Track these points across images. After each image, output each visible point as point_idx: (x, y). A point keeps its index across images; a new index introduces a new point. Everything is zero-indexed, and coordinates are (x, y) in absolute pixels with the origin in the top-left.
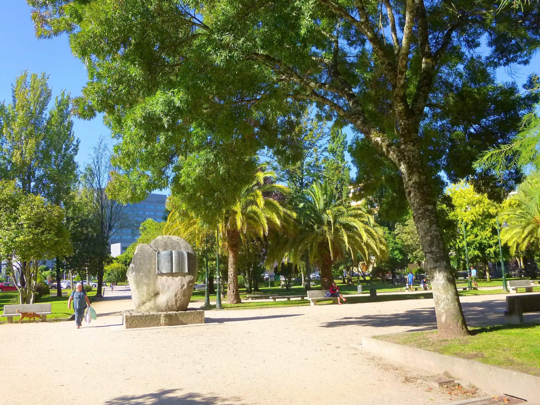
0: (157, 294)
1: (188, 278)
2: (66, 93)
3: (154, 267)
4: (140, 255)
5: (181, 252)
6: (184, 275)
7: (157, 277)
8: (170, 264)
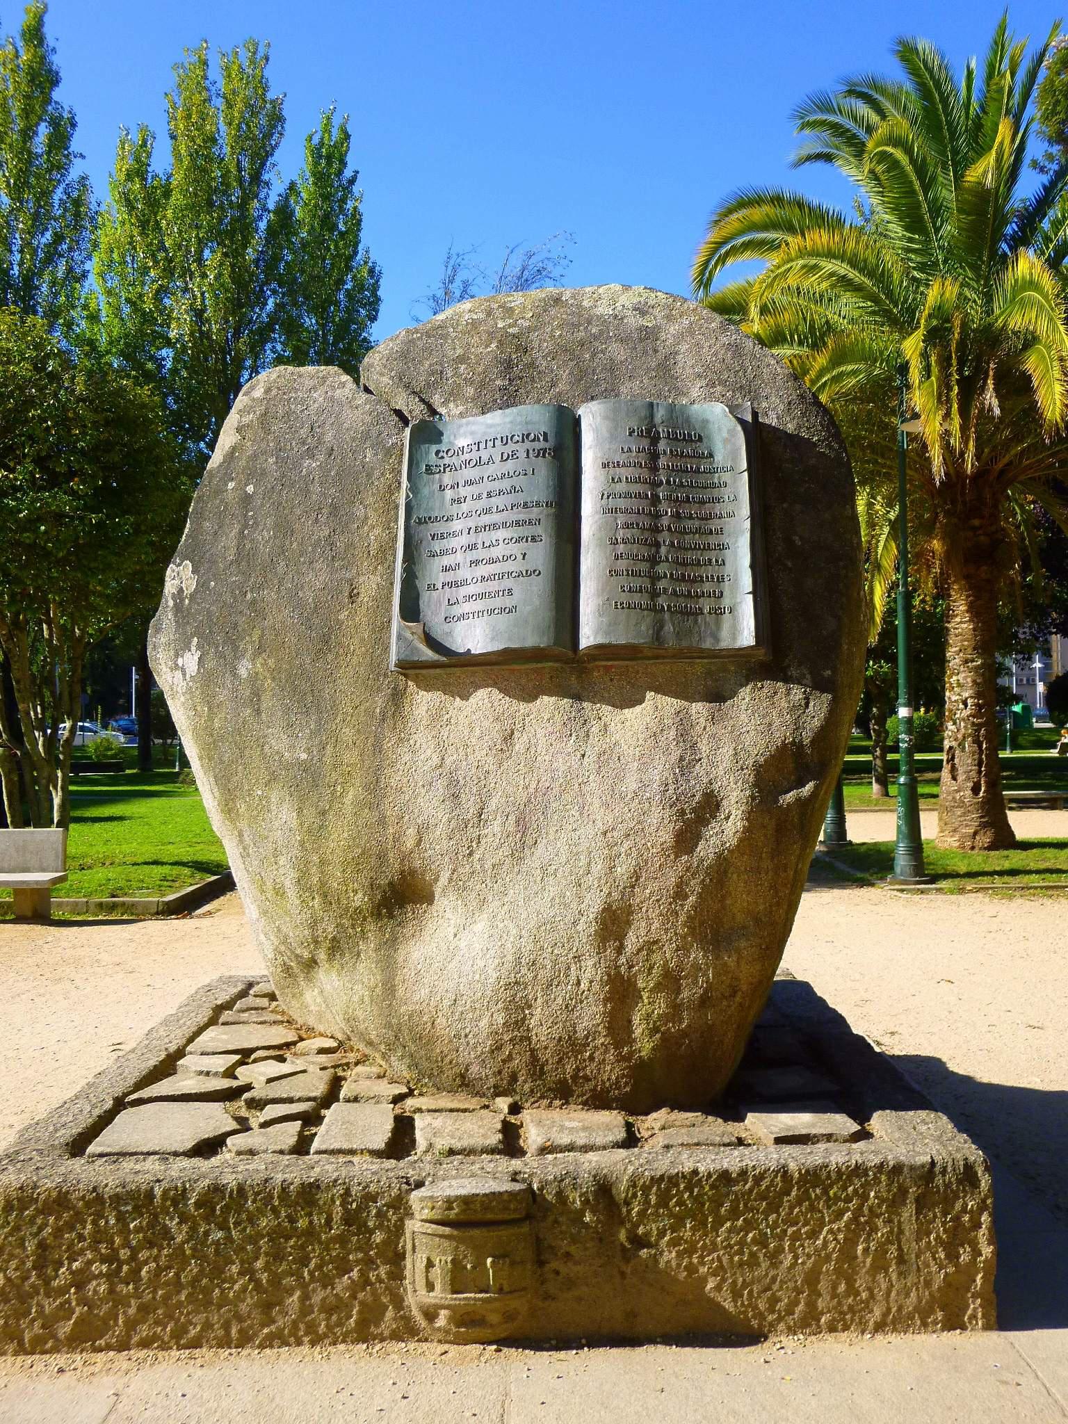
0: (400, 896)
1: (760, 719)
2: (337, 121)
3: (369, 585)
4: (255, 474)
5: (677, 417)
6: (715, 679)
7: (397, 697)
8: (541, 555)
